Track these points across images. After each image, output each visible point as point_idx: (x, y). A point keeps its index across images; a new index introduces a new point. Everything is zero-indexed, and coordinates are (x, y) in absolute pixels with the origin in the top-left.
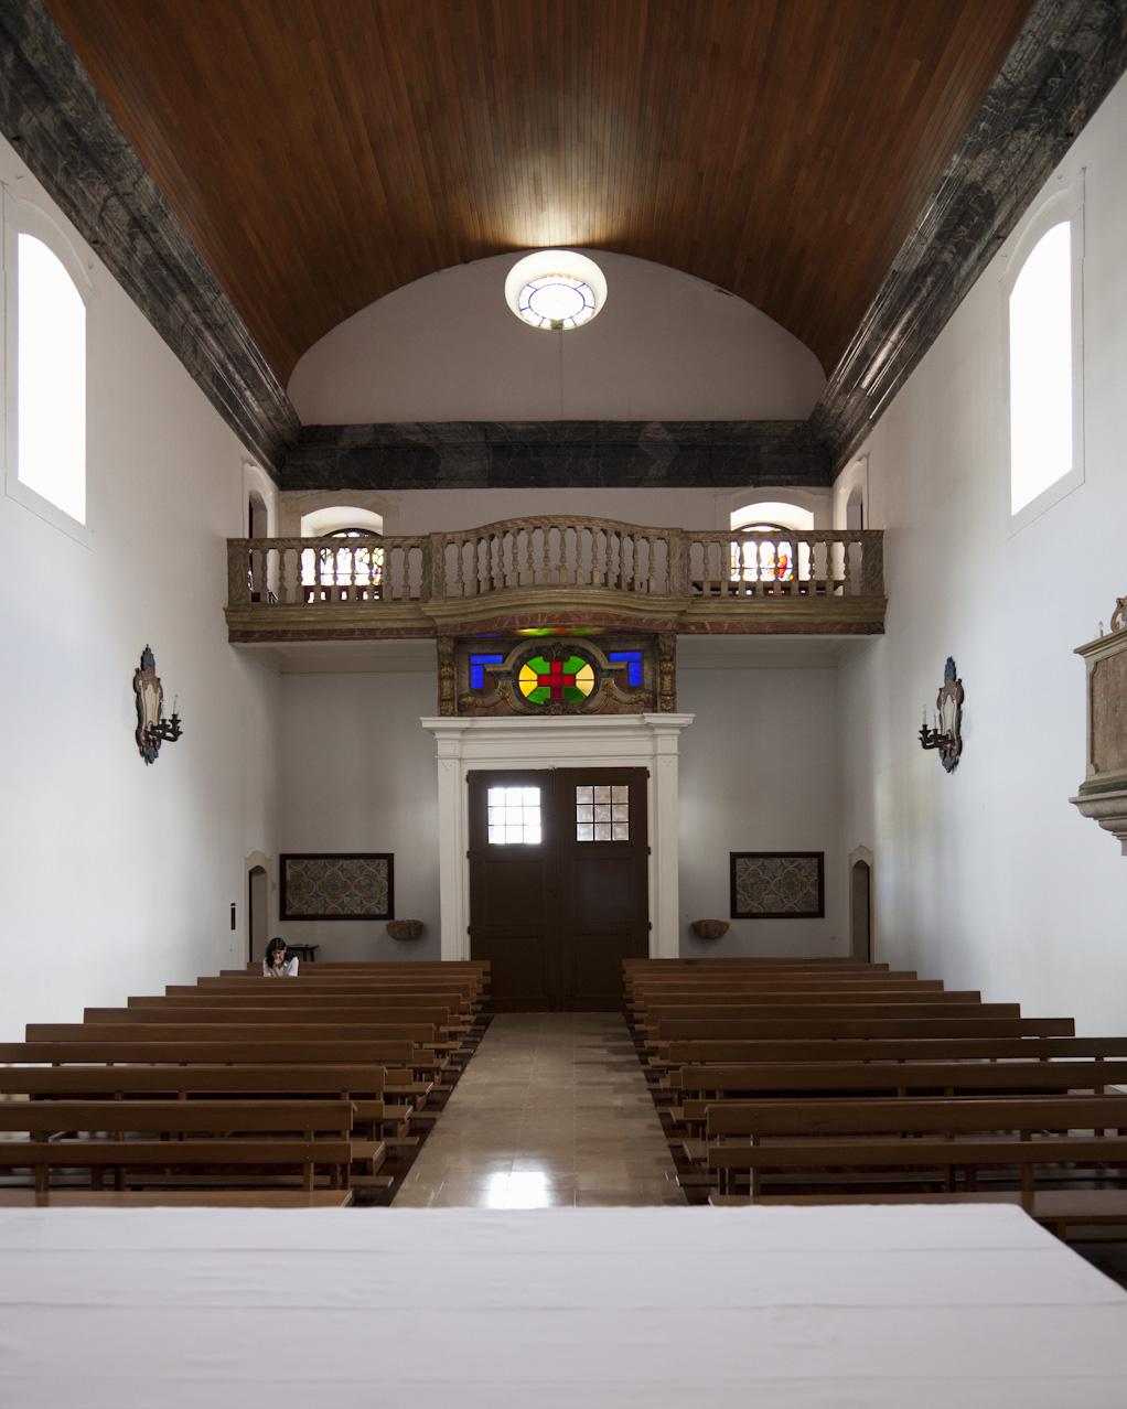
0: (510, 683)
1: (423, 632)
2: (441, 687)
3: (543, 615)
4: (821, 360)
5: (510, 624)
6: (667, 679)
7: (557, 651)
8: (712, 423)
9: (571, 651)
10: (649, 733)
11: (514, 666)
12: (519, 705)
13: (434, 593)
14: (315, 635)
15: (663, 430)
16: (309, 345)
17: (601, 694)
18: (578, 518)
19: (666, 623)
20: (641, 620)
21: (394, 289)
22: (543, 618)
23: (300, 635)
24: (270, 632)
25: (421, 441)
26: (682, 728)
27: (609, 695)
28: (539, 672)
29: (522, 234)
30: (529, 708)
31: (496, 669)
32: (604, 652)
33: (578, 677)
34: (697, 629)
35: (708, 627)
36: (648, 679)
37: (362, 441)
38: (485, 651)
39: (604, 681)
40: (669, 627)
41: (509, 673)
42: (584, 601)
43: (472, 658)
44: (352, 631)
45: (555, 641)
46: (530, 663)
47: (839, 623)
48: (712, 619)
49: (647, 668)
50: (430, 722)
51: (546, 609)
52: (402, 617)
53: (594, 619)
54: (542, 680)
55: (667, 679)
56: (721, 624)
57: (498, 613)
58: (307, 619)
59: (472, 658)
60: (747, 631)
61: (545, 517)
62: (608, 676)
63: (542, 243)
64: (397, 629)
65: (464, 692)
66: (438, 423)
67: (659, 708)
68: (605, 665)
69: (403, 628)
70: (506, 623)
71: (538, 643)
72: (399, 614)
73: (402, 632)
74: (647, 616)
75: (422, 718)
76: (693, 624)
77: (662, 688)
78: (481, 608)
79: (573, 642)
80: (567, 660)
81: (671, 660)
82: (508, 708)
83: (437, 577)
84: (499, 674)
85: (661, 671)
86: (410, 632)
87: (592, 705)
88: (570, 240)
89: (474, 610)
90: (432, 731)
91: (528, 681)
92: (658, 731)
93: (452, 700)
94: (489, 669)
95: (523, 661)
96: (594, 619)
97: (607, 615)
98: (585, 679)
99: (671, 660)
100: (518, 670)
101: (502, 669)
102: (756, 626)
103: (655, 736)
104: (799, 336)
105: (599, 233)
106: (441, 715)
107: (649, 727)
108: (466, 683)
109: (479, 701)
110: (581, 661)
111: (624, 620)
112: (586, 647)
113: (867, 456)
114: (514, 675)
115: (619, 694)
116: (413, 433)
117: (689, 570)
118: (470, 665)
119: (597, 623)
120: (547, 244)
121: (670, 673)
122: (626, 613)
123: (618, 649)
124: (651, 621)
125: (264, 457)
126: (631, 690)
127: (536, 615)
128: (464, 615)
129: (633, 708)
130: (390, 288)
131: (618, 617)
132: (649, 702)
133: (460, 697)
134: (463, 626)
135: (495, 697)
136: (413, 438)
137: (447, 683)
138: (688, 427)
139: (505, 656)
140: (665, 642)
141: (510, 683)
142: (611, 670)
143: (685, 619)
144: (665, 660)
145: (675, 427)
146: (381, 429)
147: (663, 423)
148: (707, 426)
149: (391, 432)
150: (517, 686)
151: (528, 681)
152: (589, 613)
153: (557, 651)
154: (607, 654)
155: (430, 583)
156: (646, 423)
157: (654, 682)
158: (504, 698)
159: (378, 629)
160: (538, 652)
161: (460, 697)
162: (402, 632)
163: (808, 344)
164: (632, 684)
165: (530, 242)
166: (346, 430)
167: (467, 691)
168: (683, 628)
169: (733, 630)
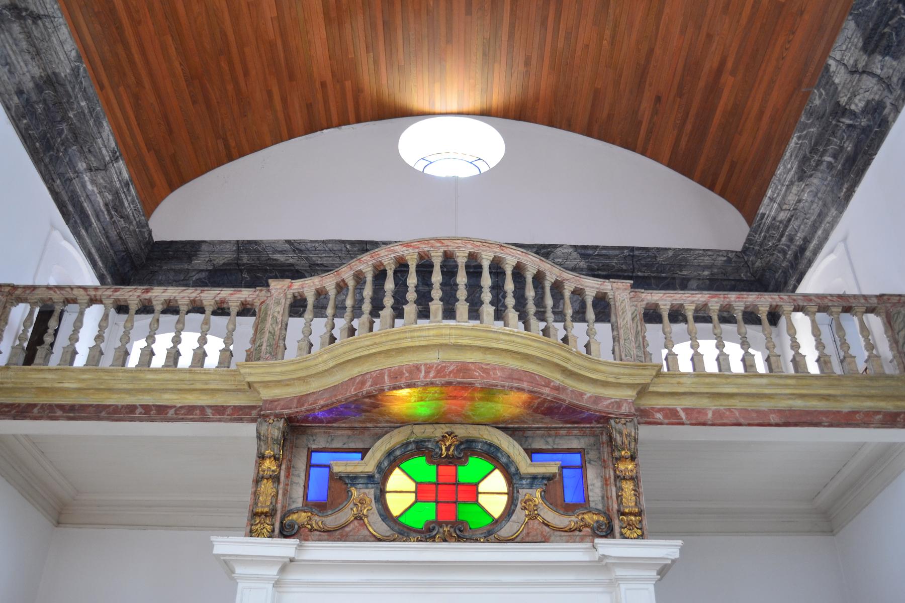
0: (370, 493)
1: (240, 414)
2: (256, 494)
4: (740, 207)
5: (374, 383)
8: (632, 249)
9: (468, 448)
11: (379, 466)
12: (382, 528)
13: (263, 354)
14: (74, 412)
15: (575, 254)
16: (183, 181)
17: (520, 515)
18: (484, 242)
19: (619, 404)
21: (282, 140)
22: (427, 372)
23: (50, 412)
24: (7, 406)
25: (291, 261)
26: (664, 570)
27: (533, 517)
28: (418, 480)
29: (417, 99)
30: (401, 531)
32: (526, 450)
33: (481, 488)
34: (665, 417)
35: (683, 415)
37: (220, 260)
38: (336, 444)
40: (625, 409)
41: (370, 478)
42: (495, 345)
43: (314, 455)
44: (131, 409)
45: (446, 429)
47: (878, 413)
48: (689, 402)
49: (592, 474)
50: (228, 545)
51: (433, 358)
52: (212, 386)
54: (422, 491)
55: (628, 487)
56: (701, 411)
58: (66, 385)
59: (314, 455)
60: (742, 421)
61: (438, 240)
62: (531, 486)
63: (438, 108)
64: (202, 408)
65: (294, 506)
66: (312, 242)
67: (617, 534)
68: (525, 465)
69: (210, 407)
70: (369, 384)
71: (420, 432)
72: (206, 382)
73: (209, 411)
74: (590, 391)
75: (213, 538)
76: (660, 410)
77: (620, 503)
80: (464, 462)
81: (633, 458)
84: (353, 479)
85: (617, 477)
86: (220, 413)
87: (506, 530)
88: (466, 108)
89: (322, 368)
90: (227, 564)
92: (620, 572)
93: (271, 514)
94: (338, 468)
95: (393, 460)
97: (531, 376)
98: (493, 495)
99: (633, 458)
100: (385, 473)
101: (359, 469)
102: (754, 415)
103: (613, 584)
104: (712, 188)
105: (497, 98)
107: (603, 564)
108: (298, 493)
109: (317, 521)
110: (487, 466)
111: (557, 389)
112: (496, 442)
113: (844, 240)
114: (377, 481)
116: (281, 252)
117: (644, 337)
118: (310, 465)
120: (444, 111)
122: (558, 378)
124: (597, 399)
125: (93, 251)
126: (568, 509)
127: (417, 368)
128: (303, 379)
129: (571, 533)
130: (278, 139)
131: (548, 383)
132: (599, 528)
133: (287, 513)
134: (301, 400)
135: (345, 515)
136: (280, 258)
137: (267, 487)
138: (604, 252)
139: (364, 452)
140: (621, 430)
141: (370, 493)
142: (534, 478)
143: (649, 402)
144: (620, 459)
145: (590, 252)
146: (243, 246)
147: (575, 247)
148: (626, 252)
149: (257, 251)
152: (503, 369)
154: (531, 453)
155: (260, 346)
156: (555, 246)
157: (605, 498)
158: (359, 518)
159: (171, 407)
160: (419, 448)
161: (287, 513)
162: (209, 411)
163: (722, 194)
164: (569, 498)
165: (426, 108)
166: (204, 247)
167: (299, 503)
168: (644, 416)
169: (719, 421)
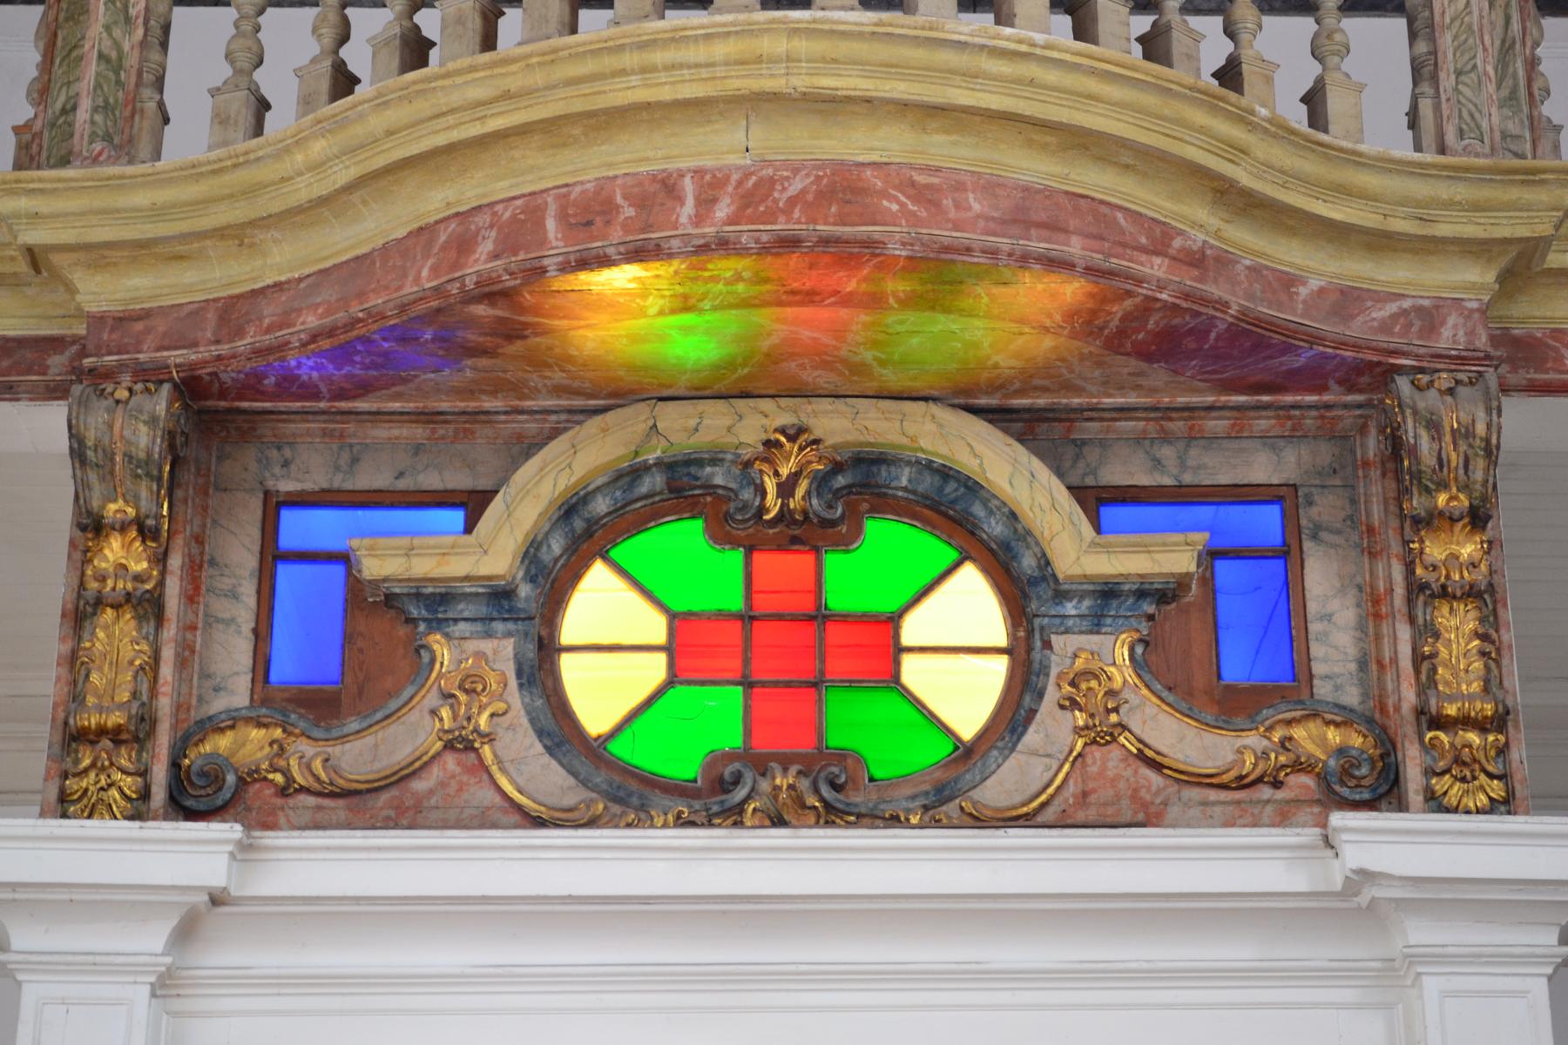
0: (501, 652)
3: (711, 185)
6: (1457, 625)
7: (790, 503)
9: (860, 488)
10: (1357, 950)
11: (531, 554)
12: (548, 779)
17: (1053, 729)
19: (1429, 317)
20: (1289, 282)
22: (706, 203)
27: (1101, 736)
28: (677, 606)
31: (423, 567)
36: (1334, 647)
39: (1068, 649)
41: (499, 597)
46: (623, 552)
49: (1324, 580)
53: (1020, 220)
55: (1457, 625)
57: (434, 200)
59: (289, 518)
62: (1095, 623)
65: (218, 705)
68: (1072, 546)
70: (486, 247)
74: (1319, 267)
78: (343, 174)
79: (877, 425)
80: (848, 539)
81: (1478, 518)
82: (488, 796)
83: (112, 63)
84: (437, 602)
85: (1416, 589)
91: (613, 641)
93: (138, 733)
95: (586, 532)
96: (1020, 220)
98: (957, 646)
100: (556, 586)
101: (457, 567)
106: (64, 805)
107: (1358, 903)
108: (233, 656)
109: (307, 756)
111: (1196, 260)
112: (966, 462)
114: (529, 609)
115: (1162, 727)
119: (1038, 246)
121: (1472, 593)
122: (1199, 220)
123: (1143, 478)
124: (1348, 299)
126: (1232, 706)
127: (668, 186)
129: (1241, 794)
131: (1160, 238)
132: (1346, 773)
133: (193, 733)
135: (410, 733)
137: (116, 636)
140: (1436, 417)
141: (501, 652)
144: (1428, 522)
150: (540, 667)
151: (613, 641)
152: (991, 187)
153: (790, 503)
154: (1096, 500)
157: (1371, 664)
160: (682, 488)
161: (193, 733)
164: (1237, 668)
167: (238, 695)
